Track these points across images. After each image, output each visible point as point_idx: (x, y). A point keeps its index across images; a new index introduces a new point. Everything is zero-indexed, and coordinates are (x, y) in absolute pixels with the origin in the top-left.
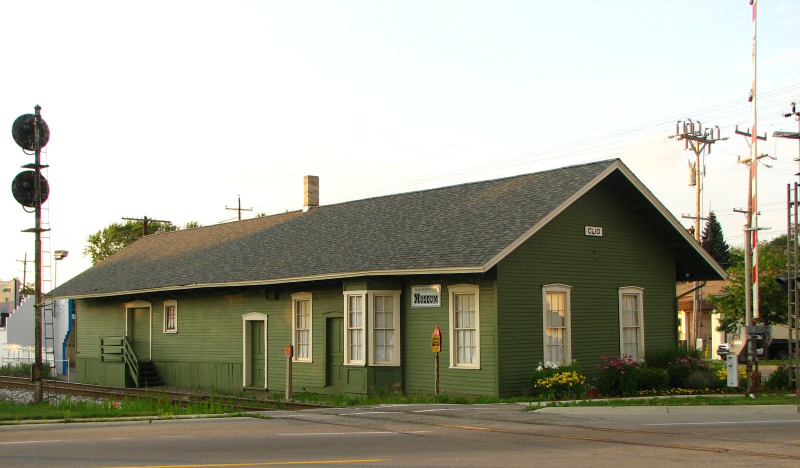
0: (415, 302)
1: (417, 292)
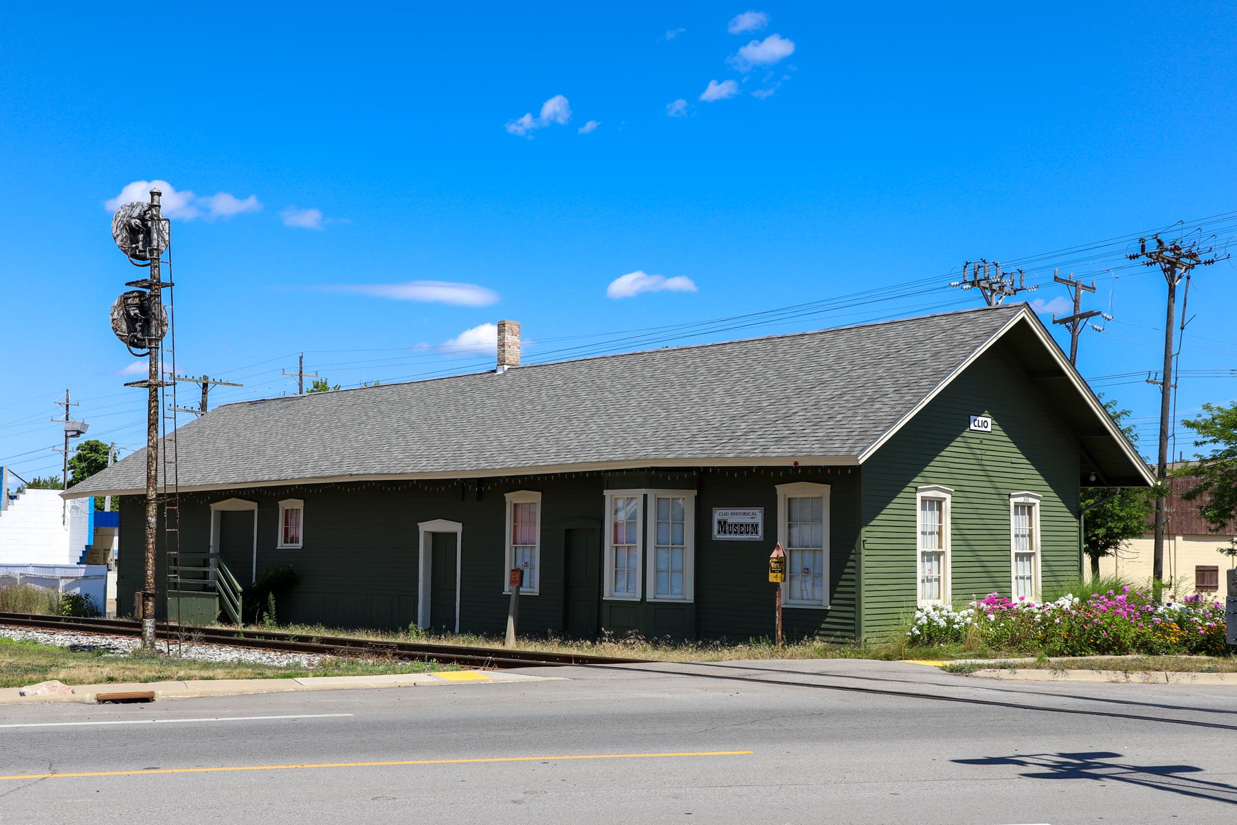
0: (719, 532)
1: (724, 518)
